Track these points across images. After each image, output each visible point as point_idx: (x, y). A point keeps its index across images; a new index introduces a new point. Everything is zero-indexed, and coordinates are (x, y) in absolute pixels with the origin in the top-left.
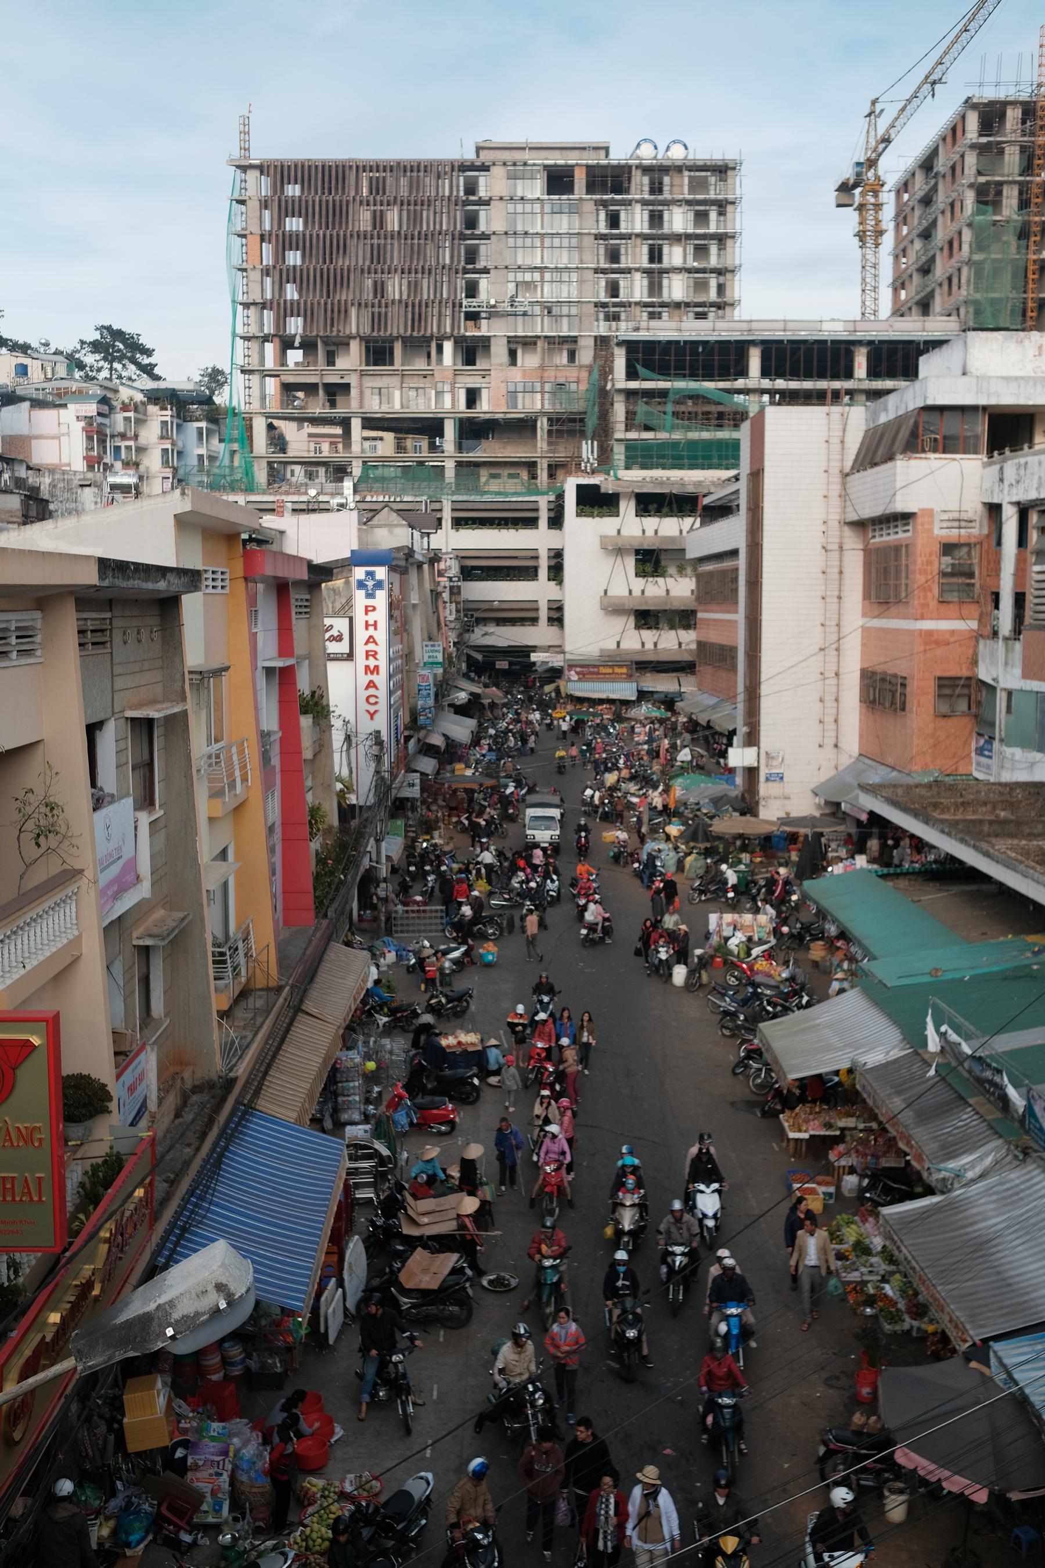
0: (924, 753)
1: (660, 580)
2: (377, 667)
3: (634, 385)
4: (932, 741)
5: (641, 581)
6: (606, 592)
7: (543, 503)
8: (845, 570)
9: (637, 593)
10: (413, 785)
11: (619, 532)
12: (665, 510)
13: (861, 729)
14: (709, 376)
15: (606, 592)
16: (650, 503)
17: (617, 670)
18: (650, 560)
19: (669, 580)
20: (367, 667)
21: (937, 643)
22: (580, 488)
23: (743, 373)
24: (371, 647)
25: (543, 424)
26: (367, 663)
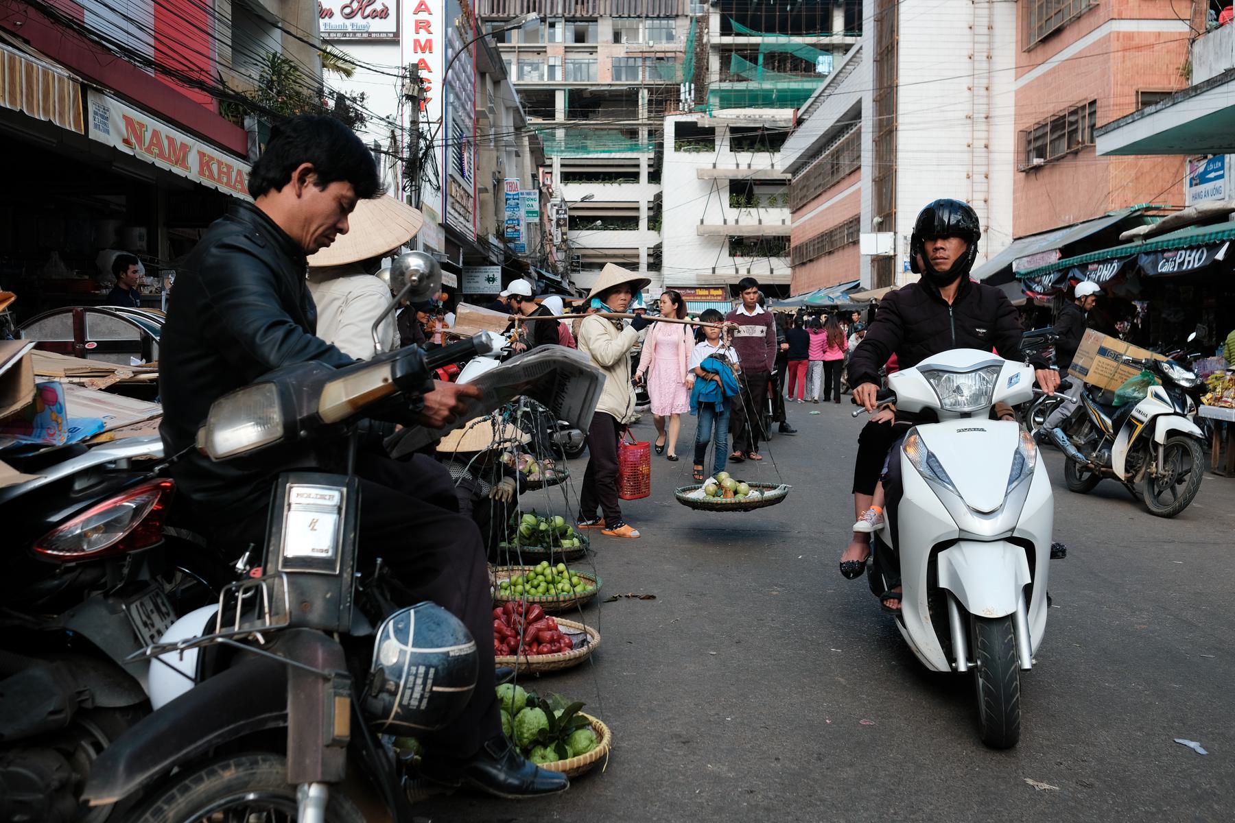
0: (1124, 187)
1: (753, 211)
2: (429, 42)
3: (728, 40)
4: (1133, 173)
5: (735, 211)
6: (702, 222)
7: (644, 159)
8: (996, 26)
9: (731, 222)
10: (493, 280)
11: (714, 166)
12: (757, 146)
13: (1016, 209)
14: (797, 32)
15: (702, 222)
16: (744, 139)
17: (713, 292)
18: (743, 192)
19: (762, 211)
20: (417, 42)
21: (1139, 48)
22: (679, 126)
23: (827, 29)
24: (423, 16)
25: (644, 96)
26: (417, 37)
